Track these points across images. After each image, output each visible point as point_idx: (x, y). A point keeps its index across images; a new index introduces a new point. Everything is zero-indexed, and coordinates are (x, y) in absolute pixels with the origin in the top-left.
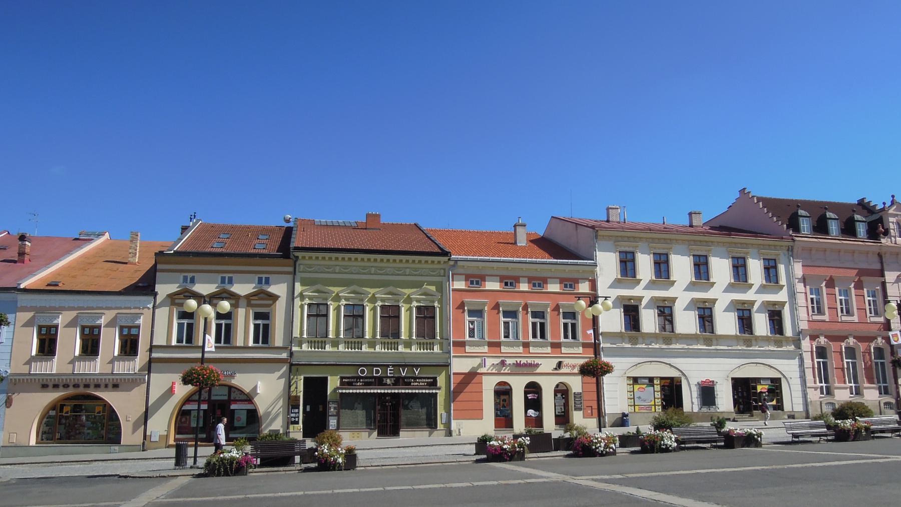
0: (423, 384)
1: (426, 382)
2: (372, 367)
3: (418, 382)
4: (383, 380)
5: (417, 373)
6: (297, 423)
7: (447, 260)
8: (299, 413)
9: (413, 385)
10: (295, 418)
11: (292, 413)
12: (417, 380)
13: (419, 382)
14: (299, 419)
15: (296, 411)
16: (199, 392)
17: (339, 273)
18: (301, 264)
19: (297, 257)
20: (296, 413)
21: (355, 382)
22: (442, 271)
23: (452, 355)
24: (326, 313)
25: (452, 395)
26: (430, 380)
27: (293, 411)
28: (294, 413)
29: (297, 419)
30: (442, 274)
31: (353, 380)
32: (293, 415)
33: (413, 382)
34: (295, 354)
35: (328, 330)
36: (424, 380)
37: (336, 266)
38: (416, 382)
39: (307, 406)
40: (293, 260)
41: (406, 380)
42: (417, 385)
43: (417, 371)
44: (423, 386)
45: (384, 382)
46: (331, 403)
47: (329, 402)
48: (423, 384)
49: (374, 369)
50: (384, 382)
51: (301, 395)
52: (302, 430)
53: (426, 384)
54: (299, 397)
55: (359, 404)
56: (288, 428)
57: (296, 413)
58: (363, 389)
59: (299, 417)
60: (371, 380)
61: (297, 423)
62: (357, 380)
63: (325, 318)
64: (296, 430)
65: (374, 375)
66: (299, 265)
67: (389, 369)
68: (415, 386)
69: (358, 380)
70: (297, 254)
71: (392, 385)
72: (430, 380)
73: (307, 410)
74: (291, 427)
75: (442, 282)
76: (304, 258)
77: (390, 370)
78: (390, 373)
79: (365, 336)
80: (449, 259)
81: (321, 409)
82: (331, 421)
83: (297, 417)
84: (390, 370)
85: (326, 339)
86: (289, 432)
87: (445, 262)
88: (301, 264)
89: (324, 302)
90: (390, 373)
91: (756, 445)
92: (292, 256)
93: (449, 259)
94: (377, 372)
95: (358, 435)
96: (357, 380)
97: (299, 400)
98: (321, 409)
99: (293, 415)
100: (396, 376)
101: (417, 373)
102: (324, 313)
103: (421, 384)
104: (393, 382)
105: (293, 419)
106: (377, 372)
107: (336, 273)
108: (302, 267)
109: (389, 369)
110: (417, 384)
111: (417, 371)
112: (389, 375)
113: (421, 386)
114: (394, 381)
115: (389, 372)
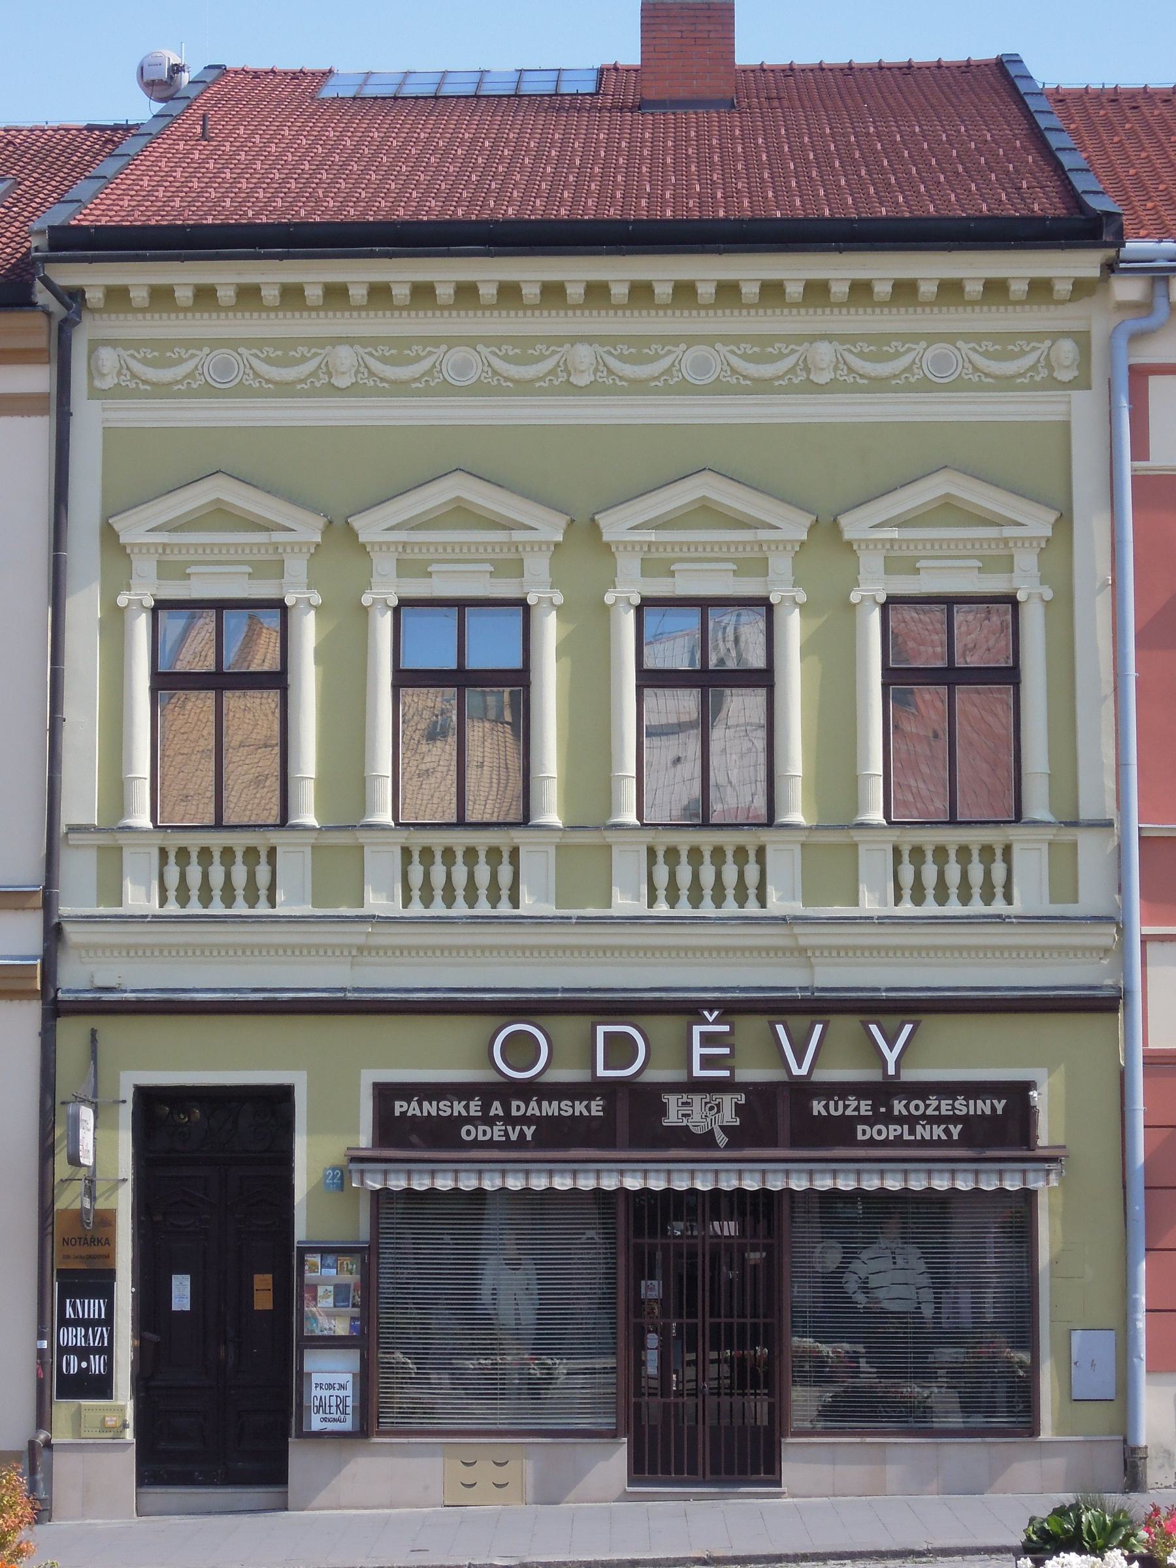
0: (938, 1132)
1: (954, 1119)
2: (584, 1021)
3: (900, 1120)
4: (663, 1110)
5: (891, 1057)
6: (101, 1387)
7: (1096, 273)
8: (108, 1321)
9: (872, 1143)
10: (83, 1353)
11: (64, 1322)
12: (898, 1107)
13: (911, 1121)
14: (109, 1365)
15: (93, 1308)
16: (1028, 1367)
17: (352, 391)
18: (107, 342)
19: (74, 298)
20: (87, 1323)
21: (470, 1120)
22: (1067, 349)
23: (1138, 929)
24: (518, 664)
25: (1138, 1207)
26: (983, 1107)
27: (69, 1312)
28: (76, 1323)
29: (96, 1365)
30: (1065, 376)
31: (459, 1108)
32: (72, 1337)
33: (869, 1121)
34: (72, 933)
35: (292, 773)
36: (945, 1107)
37: (814, 338)
38: (889, 1119)
39: (269, 1306)
40: (49, 314)
41: (817, 1107)
42: (899, 1142)
43: (891, 1047)
44: (939, 1143)
45: (673, 1118)
46: (316, 1259)
47: (303, 1251)
48: (938, 1132)
49: (601, 1030)
50: (673, 1118)
51: (123, 1204)
52: (129, 1435)
53: (956, 1131)
54: (107, 1220)
55: (514, 1265)
56: (43, 1419)
57: (87, 1323)
58: (526, 1166)
59: (107, 1351)
60: (580, 1108)
61: (101, 1387)
62: (486, 1107)
63: (273, 696)
64: (91, 1434)
65: (601, 1072)
66: (94, 346)
67: (697, 1030)
68: (886, 1143)
69: (496, 1109)
70: (67, 275)
71: (721, 1139)
72: (983, 1107)
73: (175, 1307)
74: (63, 1410)
75: (1066, 426)
76: (117, 296)
77: (707, 1040)
78: (707, 1062)
79: (542, 812)
80: (1110, 267)
81: (263, 1301)
82: (316, 1379)
83: (100, 1351)
84: (707, 1040)
85: (518, 836)
86: (48, 1445)
87: (1082, 288)
88: (107, 342)
89: (505, 589)
90: (707, 1062)
91: (110, 1225)
92: (42, 296)
93: (1110, 267)
94: (620, 1049)
95: (501, 1475)
96: (486, 1107)
97: (109, 1242)
98: (263, 1301)
99: (72, 1337)
100: (748, 1074)
101: (891, 1057)
102: (264, 659)
103: (923, 1132)
104: (728, 1116)
105: (73, 1365)
106: (620, 1049)
107: (333, 391)
108: (108, 357)
109: (697, 1030)
110: (893, 1131)
111: (891, 1047)
112: (697, 1072)
113: (923, 1143)
114: (739, 1110)
115: (698, 1051)
